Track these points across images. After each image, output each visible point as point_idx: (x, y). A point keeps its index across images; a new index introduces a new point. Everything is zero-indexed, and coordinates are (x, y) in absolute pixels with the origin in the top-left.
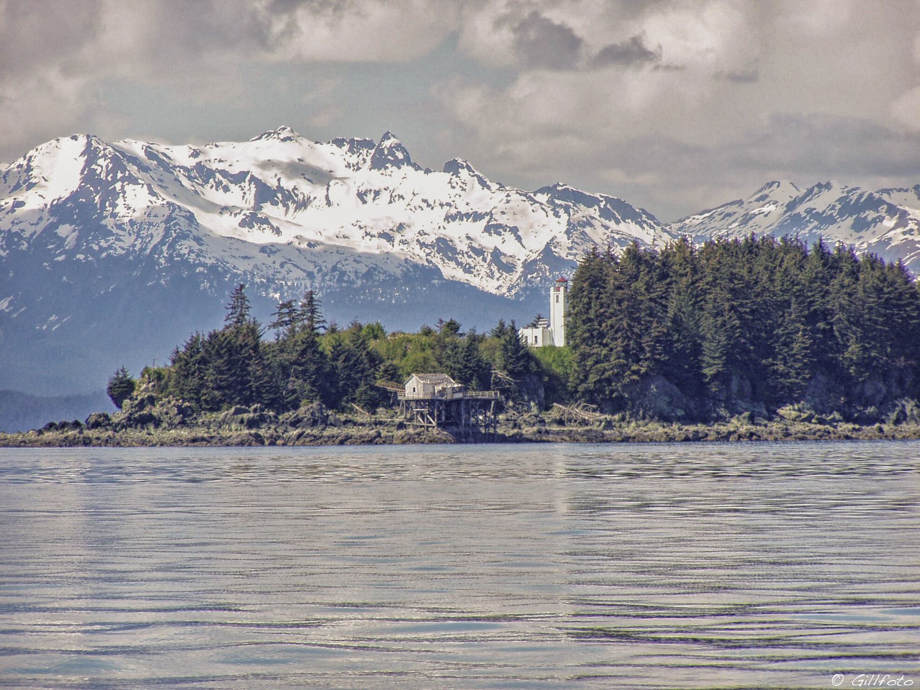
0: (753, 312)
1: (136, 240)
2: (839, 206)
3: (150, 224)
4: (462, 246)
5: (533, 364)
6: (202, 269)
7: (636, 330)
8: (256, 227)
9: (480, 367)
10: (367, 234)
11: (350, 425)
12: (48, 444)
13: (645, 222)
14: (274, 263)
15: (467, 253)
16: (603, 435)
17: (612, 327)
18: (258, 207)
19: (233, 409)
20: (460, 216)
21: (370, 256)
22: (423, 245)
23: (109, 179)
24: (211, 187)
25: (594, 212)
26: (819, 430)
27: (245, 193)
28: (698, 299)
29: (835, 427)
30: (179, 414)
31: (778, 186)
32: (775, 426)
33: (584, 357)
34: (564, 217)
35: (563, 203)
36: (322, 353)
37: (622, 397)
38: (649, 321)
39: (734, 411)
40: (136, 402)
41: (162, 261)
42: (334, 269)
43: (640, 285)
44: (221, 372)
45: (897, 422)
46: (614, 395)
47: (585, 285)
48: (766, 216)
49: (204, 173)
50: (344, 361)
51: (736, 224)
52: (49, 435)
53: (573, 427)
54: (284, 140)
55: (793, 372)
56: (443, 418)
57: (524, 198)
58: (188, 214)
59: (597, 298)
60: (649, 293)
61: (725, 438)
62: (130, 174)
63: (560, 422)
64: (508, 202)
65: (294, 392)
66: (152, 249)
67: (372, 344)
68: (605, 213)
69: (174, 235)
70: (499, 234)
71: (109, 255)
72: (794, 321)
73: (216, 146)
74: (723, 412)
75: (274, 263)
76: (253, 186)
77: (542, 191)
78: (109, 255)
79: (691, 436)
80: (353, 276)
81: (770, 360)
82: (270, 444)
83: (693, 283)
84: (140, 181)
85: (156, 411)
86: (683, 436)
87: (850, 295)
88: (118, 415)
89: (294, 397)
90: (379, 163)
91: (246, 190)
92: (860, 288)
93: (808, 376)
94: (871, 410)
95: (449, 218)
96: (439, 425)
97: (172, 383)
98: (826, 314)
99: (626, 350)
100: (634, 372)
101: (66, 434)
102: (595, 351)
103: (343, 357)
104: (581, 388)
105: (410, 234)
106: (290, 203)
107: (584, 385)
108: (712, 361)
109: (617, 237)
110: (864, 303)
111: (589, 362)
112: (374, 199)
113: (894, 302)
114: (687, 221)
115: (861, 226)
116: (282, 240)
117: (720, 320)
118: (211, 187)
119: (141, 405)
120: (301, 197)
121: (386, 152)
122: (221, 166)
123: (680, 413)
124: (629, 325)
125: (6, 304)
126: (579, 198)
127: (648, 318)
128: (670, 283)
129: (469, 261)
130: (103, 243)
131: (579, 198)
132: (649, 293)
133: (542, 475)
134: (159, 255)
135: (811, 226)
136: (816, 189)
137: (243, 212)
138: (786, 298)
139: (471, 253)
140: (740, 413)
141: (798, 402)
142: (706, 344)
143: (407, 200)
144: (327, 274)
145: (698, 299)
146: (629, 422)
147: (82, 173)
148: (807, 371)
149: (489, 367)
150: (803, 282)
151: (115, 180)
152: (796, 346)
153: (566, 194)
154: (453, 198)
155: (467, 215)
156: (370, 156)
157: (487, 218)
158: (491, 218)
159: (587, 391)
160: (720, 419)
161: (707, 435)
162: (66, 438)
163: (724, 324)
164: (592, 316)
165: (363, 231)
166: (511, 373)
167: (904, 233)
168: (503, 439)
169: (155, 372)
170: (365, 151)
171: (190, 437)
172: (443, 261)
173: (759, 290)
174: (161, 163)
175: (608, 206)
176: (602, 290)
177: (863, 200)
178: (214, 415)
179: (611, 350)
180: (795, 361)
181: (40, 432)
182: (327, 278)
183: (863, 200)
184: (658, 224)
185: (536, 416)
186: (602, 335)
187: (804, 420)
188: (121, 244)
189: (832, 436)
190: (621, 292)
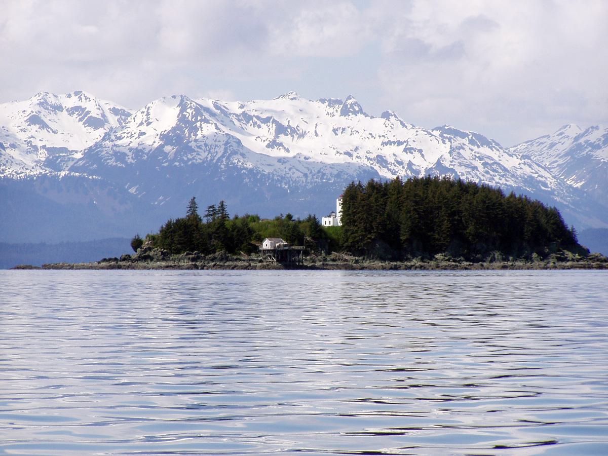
0: (424, 211)
1: (208, 155)
2: (603, 139)
3: (216, 146)
4: (391, 160)
5: (323, 234)
6: (245, 171)
7: (370, 219)
8: (276, 148)
9: (300, 235)
10: (338, 152)
11: (238, 261)
12: (102, 268)
13: (494, 147)
14: (285, 168)
15: (393, 164)
16: (352, 266)
17: (359, 217)
18: (277, 136)
19: (185, 253)
20: (390, 143)
21: (339, 165)
22: (369, 159)
23: (193, 120)
24: (251, 125)
25: (465, 141)
26: (453, 265)
27: (269, 129)
28: (399, 205)
29: (460, 263)
30: (161, 255)
31: (570, 127)
32: (433, 263)
33: (347, 231)
34: (448, 144)
35: (448, 136)
36: (226, 229)
37: (364, 249)
38: (377, 216)
39: (414, 256)
40: (143, 249)
41: (223, 166)
42: (319, 172)
43: (372, 199)
44: (181, 237)
45: (491, 261)
46: (360, 248)
47: (348, 199)
48: (562, 144)
49: (246, 117)
50: (237, 232)
51: (546, 148)
52: (103, 264)
53: (339, 263)
54: (292, 99)
55: (442, 239)
57: (426, 133)
58: (237, 141)
59: (353, 205)
60: (376, 203)
61: (409, 268)
62: (205, 117)
63: (334, 260)
64: (417, 135)
65: (213, 245)
66: (218, 159)
67: (251, 225)
68: (472, 142)
69: (229, 152)
70: (412, 153)
71: (192, 162)
72: (443, 216)
73: (254, 102)
74: (409, 256)
75: (285, 168)
76: (274, 125)
77: (437, 129)
78: (192, 162)
79: (393, 267)
80: (329, 176)
81: (432, 233)
82: (201, 269)
83: (398, 198)
84: (210, 122)
85: (151, 253)
86: (390, 267)
87: (470, 204)
88: (134, 255)
89: (213, 248)
90: (345, 112)
91: (270, 127)
92: (475, 202)
93: (449, 241)
94: (479, 256)
95: (384, 144)
96: (277, 261)
97: (159, 241)
98: (460, 212)
99: (365, 228)
100: (369, 238)
101: (110, 264)
102: (351, 228)
103: (236, 230)
104: (345, 245)
105: (362, 153)
106: (295, 135)
107: (346, 244)
108: (404, 234)
109: (478, 155)
110: (477, 207)
111: (349, 233)
112: (342, 133)
113: (491, 207)
114: (519, 147)
116: (291, 155)
117: (409, 215)
118: (251, 125)
119: (145, 251)
120: (301, 131)
121: (349, 106)
122: (256, 114)
123: (390, 256)
124: (367, 217)
125: (135, 190)
126: (457, 133)
127: (375, 214)
128: (388, 198)
129: (395, 168)
130: (189, 156)
131: (457, 133)
132: (376, 203)
133: (326, 284)
134: (221, 163)
135: (587, 150)
136: (590, 130)
137: (268, 140)
138: (440, 205)
139: (396, 164)
140: (417, 257)
141: (444, 252)
142: (402, 226)
143: (361, 133)
144: (314, 175)
145: (399, 205)
146: (366, 260)
147: (178, 117)
148: (448, 238)
149: (303, 235)
150: (449, 198)
151: (196, 121)
152: (444, 227)
153: (450, 131)
154: (386, 133)
155: (394, 143)
156: (340, 109)
157: (405, 144)
158: (407, 144)
159: (347, 247)
160: (408, 260)
161: (400, 267)
162: (110, 265)
163: (410, 217)
165: (336, 150)
166: (313, 238)
168: (306, 268)
169: (152, 236)
170: (337, 105)
171: (165, 265)
172: (380, 167)
173: (427, 201)
174: (222, 111)
175: (474, 138)
176: (355, 201)
178: (178, 256)
179: (358, 228)
180: (443, 234)
181: (99, 263)
182: (315, 177)
184: (501, 148)
185: (324, 257)
186: (355, 221)
187: (446, 260)
188: (199, 157)
189: (459, 268)
190: (364, 202)
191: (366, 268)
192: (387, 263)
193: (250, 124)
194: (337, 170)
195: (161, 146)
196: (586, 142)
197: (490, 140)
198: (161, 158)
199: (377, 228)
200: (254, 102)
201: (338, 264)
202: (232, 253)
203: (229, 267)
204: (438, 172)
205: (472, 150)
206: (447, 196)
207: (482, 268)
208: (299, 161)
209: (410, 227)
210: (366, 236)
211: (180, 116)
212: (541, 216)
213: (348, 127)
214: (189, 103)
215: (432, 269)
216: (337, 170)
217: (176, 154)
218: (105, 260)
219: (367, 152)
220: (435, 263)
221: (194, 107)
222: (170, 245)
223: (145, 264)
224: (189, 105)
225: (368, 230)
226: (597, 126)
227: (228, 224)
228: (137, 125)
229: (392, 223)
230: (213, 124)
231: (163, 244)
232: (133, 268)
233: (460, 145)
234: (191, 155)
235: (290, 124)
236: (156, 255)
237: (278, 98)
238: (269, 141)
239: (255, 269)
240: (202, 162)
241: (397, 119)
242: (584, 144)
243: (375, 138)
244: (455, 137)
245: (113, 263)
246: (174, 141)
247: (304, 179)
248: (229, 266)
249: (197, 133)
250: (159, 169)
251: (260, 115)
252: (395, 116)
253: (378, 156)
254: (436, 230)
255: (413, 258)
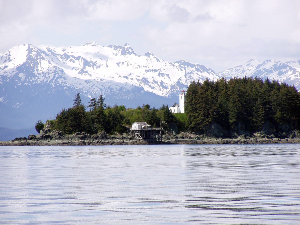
0: (245, 102)
1: (44, 78)
2: (273, 67)
3: (49, 73)
4: (150, 80)
5: (174, 119)
6: (66, 88)
7: (207, 108)
8: (84, 74)
9: (157, 120)
10: (120, 76)
13: (210, 72)
14: (89, 86)
15: (152, 82)
17: (200, 106)
18: (84, 68)
19: (76, 133)
21: (121, 84)
22: (138, 80)
23: (36, 58)
24: (69, 61)
25: (194, 69)
26: (267, 140)
27: (80, 63)
28: (227, 97)
29: (272, 139)
30: (58, 135)
31: (254, 61)
32: (253, 139)
33: (190, 116)
34: (184, 71)
35: (184, 66)
36: (105, 115)
37: (203, 130)
38: (212, 105)
39: (239, 134)
41: (53, 85)
42: (109, 88)
43: (209, 93)
44: (72, 121)
45: (293, 138)
46: (200, 129)
47: (191, 93)
48: (250, 70)
49: (67, 57)
50: (112, 118)
51: (240, 73)
52: (16, 142)
54: (93, 46)
56: (145, 136)
57: (171, 65)
58: (61, 70)
59: (195, 97)
60: (212, 95)
61: (236, 143)
63: (183, 138)
64: (166, 66)
65: (96, 128)
67: (122, 112)
68: (197, 70)
69: (57, 77)
70: (163, 76)
72: (259, 105)
73: (71, 48)
74: (236, 134)
76: (82, 61)
77: (177, 62)
78: (36, 83)
79: (225, 142)
80: (115, 90)
81: (251, 117)
82: (88, 145)
83: (226, 92)
84: (46, 59)
85: (51, 134)
86: (223, 142)
88: (38, 135)
89: (96, 129)
90: (124, 53)
91: (80, 62)
93: (263, 123)
94: (284, 134)
95: (146, 71)
96: (143, 139)
97: (56, 125)
98: (269, 102)
99: (204, 114)
101: (21, 142)
102: (194, 114)
103: (112, 116)
104: (189, 127)
105: (134, 76)
107: (191, 126)
108: (232, 118)
109: (201, 77)
111: (192, 118)
112: (122, 65)
113: (292, 98)
114: (224, 72)
115: (280, 74)
117: (235, 104)
118: (69, 61)
119: (46, 132)
120: (98, 64)
121: (126, 50)
122: (72, 54)
123: (222, 135)
124: (205, 106)
125: (2, 99)
128: (219, 92)
129: (153, 85)
130: (34, 79)
131: (189, 65)
134: (52, 83)
135: (264, 74)
136: (266, 62)
137: (79, 69)
138: (256, 97)
139: (153, 82)
141: (260, 131)
142: (230, 112)
143: (133, 65)
145: (227, 97)
146: (205, 138)
147: (27, 56)
148: (263, 121)
149: (159, 120)
150: (262, 92)
151: (37, 59)
152: (260, 113)
153: (185, 63)
155: (152, 70)
156: (121, 51)
157: (159, 71)
158: (160, 71)
159: (191, 128)
161: (230, 142)
162: (22, 143)
163: (236, 106)
164: (193, 103)
165: (118, 75)
166: (167, 122)
167: (295, 76)
169: (51, 121)
170: (119, 49)
171: (62, 142)
172: (145, 85)
174: (52, 53)
175: (198, 67)
177: (281, 65)
178: (70, 135)
179: (199, 114)
180: (259, 118)
181: (13, 141)
182: (107, 91)
183: (281, 65)
184: (215, 73)
185: (175, 136)
186: (196, 109)
187: (262, 137)
188: (40, 80)
190: (203, 95)
191: (207, 143)
192: (220, 139)
193: (68, 60)
194: (120, 87)
195: (18, 74)
196: (264, 69)
197: (208, 69)
198: (17, 80)
199: (213, 114)
200: (71, 48)
201: (186, 140)
202: (110, 133)
203: (108, 144)
204: (178, 87)
205: (198, 74)
206: (261, 90)
207: (288, 142)
208: (97, 81)
209: (236, 113)
210: (204, 120)
211: (28, 56)
212: (91, 123)
213: (126, 62)
214: (33, 48)
215: (253, 143)
216: (120, 87)
217: (26, 78)
218: (17, 139)
219: (137, 76)
220: (254, 139)
221: (36, 51)
222: (64, 127)
223: (47, 142)
224: (33, 50)
225: (206, 116)
226: (270, 60)
227: (106, 113)
228: (3, 62)
229: (223, 110)
230: (47, 61)
231: (59, 127)
232: (39, 145)
233: (191, 72)
234: (34, 78)
235: (92, 60)
236: (54, 135)
237: (85, 45)
238: (80, 70)
239: (127, 145)
240: (41, 83)
241: (154, 57)
242: (263, 70)
243: (141, 68)
244: (187, 67)
245: (23, 141)
246: (25, 71)
247: (100, 92)
248: (109, 142)
249: (38, 66)
250: (16, 87)
251: (74, 55)
252: (153, 55)
253: (143, 78)
254: (254, 115)
255: (239, 136)
